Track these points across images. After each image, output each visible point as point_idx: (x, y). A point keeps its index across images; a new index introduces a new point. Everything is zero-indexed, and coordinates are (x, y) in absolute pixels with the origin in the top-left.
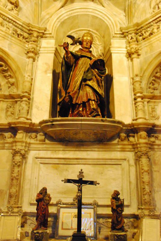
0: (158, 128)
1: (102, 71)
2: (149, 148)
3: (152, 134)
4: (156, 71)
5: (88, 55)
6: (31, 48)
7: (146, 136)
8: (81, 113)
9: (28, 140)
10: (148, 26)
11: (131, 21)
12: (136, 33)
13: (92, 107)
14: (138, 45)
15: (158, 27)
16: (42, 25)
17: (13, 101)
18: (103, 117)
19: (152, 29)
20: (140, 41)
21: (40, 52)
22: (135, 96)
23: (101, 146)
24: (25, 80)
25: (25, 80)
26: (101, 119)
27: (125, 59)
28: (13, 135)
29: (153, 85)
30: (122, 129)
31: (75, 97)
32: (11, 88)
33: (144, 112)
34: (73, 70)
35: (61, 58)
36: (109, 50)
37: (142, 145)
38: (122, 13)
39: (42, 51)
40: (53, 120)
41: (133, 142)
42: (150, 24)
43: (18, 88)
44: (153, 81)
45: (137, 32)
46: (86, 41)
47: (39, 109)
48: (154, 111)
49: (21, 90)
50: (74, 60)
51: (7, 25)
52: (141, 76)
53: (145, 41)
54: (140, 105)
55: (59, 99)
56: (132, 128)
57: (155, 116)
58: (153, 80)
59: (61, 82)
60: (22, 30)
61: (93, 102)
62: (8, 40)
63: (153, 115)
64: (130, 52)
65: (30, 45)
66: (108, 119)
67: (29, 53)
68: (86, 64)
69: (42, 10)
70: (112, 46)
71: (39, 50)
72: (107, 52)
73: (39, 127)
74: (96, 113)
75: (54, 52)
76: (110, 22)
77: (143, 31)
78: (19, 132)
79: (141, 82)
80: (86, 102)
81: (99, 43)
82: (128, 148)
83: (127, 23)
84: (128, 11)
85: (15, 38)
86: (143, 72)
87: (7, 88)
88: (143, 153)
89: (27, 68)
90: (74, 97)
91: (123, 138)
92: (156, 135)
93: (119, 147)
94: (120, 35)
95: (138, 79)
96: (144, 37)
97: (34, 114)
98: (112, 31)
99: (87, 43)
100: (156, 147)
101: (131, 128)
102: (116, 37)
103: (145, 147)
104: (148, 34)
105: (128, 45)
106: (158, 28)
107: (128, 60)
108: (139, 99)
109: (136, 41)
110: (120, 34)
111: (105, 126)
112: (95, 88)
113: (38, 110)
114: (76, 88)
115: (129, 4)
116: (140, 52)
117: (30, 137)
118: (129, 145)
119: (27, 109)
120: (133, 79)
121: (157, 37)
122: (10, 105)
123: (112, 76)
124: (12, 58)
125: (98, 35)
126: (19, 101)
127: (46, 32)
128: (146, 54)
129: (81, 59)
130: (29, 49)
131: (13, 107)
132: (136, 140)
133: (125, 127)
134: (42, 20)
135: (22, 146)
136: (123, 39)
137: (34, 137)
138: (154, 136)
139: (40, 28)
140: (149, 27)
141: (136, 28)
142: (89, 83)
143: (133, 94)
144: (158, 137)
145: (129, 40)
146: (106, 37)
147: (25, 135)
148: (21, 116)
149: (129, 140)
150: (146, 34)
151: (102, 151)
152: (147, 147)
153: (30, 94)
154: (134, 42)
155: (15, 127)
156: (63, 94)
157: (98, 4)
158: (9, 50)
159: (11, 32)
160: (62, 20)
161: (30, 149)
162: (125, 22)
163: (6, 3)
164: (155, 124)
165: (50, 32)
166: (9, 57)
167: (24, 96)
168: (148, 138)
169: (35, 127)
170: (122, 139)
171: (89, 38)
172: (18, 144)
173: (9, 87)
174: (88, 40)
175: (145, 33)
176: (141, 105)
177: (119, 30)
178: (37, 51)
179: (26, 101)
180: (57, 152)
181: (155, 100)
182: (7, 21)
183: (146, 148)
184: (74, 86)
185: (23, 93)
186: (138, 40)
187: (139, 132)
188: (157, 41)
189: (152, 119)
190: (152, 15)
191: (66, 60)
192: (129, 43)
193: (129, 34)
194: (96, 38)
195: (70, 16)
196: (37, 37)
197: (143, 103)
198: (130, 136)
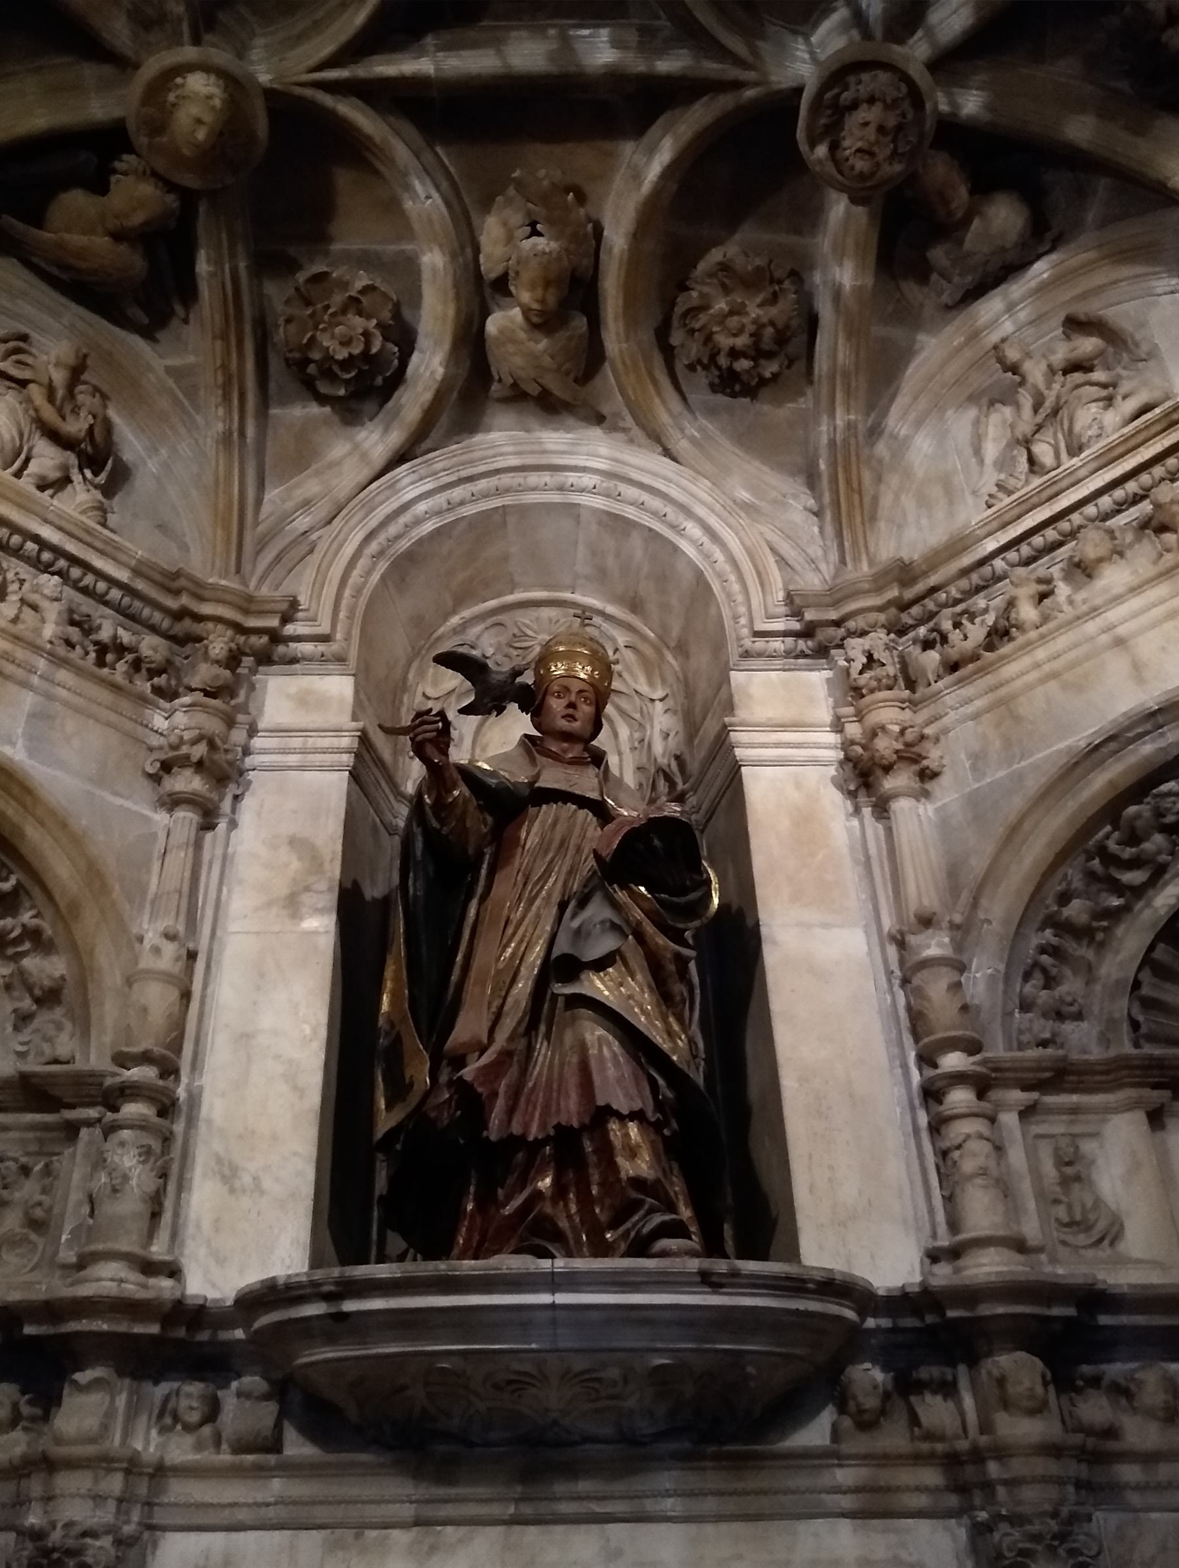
0: (1124, 1320)
1: (684, 892)
2: (1079, 1485)
3: (1086, 1369)
4: (1056, 886)
5: (586, 783)
6: (187, 736)
7: (1039, 1390)
8: (548, 1209)
9: (147, 1442)
10: (975, 578)
11: (855, 543)
12: (899, 627)
13: (627, 1168)
14: (914, 705)
15: (1043, 588)
16: (262, 579)
17: (46, 1127)
18: (713, 1248)
19: (999, 602)
20: (931, 678)
21: (249, 761)
22: (930, 1073)
23: (713, 1479)
24: (142, 965)
25: (142, 965)
26: (694, 1264)
27: (834, 803)
28: (30, 1403)
29: (1050, 982)
30: (854, 1330)
31: (502, 1089)
32: (36, 1023)
33: (1004, 1188)
34: (480, 890)
35: (399, 794)
36: (722, 745)
37: (1018, 1467)
38: (795, 497)
39: (264, 752)
40: (340, 1282)
41: (949, 1432)
42: (986, 570)
43: (84, 1025)
44: (1045, 959)
45: (906, 619)
46: (567, 689)
47: (237, 1184)
48: (1078, 1178)
49: (108, 1039)
50: (490, 819)
51: (26, 586)
52: (953, 927)
53: (960, 680)
54: (968, 1137)
55: (382, 1104)
56: (930, 1319)
57: (1092, 1217)
58: (1042, 950)
59: (397, 979)
60: (133, 618)
61: (633, 1130)
62: (25, 685)
63: (1070, 1207)
64: (866, 755)
65: (180, 718)
66: (751, 1266)
67: (175, 770)
68: (572, 851)
69: (272, 386)
70: (742, 714)
71: (247, 751)
72: (712, 756)
73: (239, 1334)
74: (658, 1219)
75: (347, 759)
76: (718, 555)
77: (948, 612)
78: (83, 1377)
79: (962, 968)
80: (583, 1127)
81: (651, 684)
82: (918, 1489)
83: (834, 556)
84: (834, 480)
85: (79, 671)
86: (965, 897)
87: (10, 1029)
88: (1036, 1538)
89: (154, 880)
90: (494, 1095)
91: (871, 1403)
92: (1115, 1370)
93: (844, 1476)
94: (790, 641)
95: (935, 945)
96: (953, 653)
97: (198, 1227)
98: (736, 618)
99: (572, 705)
100: (1130, 1473)
101: (923, 1319)
102: (760, 655)
103: (1045, 1479)
104: (976, 632)
105: (850, 710)
106: (1043, 597)
107: (857, 811)
108: (960, 1098)
109: (901, 683)
110: (786, 634)
111: (728, 1320)
112: (641, 1022)
113: (232, 1191)
114: (508, 1024)
115: (839, 437)
116: (934, 756)
117: (161, 1415)
118: (917, 1459)
119: (151, 1184)
120: (901, 944)
121: (1041, 654)
122: (24, 1160)
123: (750, 922)
124: (53, 813)
125: (644, 638)
126: (89, 1123)
127: (290, 629)
128: (974, 768)
129: (532, 810)
130: (174, 747)
131: (47, 1171)
132: (972, 1417)
133: (875, 1316)
134: (262, 544)
135: (98, 1499)
136: (810, 669)
137: (194, 1417)
138: (1105, 1383)
139: (250, 599)
140: (984, 587)
141: (893, 593)
142: (599, 986)
143: (912, 1056)
144: (1132, 1387)
145: (854, 674)
146: (701, 660)
147: (129, 1402)
148: (100, 1247)
149: (914, 1420)
150: (966, 638)
151: (719, 1518)
152: (1060, 1482)
153: (169, 1070)
154: (890, 688)
155: (48, 1338)
156: (420, 1072)
157: (631, 441)
158: (31, 752)
159: (49, 630)
160: (404, 544)
161: (159, 1518)
162: (820, 552)
163: (21, 435)
164: (1100, 1286)
165: (324, 628)
166: (28, 800)
167: (128, 1092)
168: (1059, 1392)
169: (204, 1336)
170: (861, 1411)
171: (583, 672)
172: (66, 1482)
173: (22, 1020)
174: (575, 686)
175: (957, 625)
176: (981, 1137)
177: (783, 610)
178: (230, 757)
179: (141, 1126)
180: (372, 1534)
181: (1075, 1098)
182: (27, 560)
183: (1053, 1492)
184: (494, 1009)
185: (123, 1060)
186: (911, 671)
187: (989, 1354)
188: (1043, 681)
189: (1069, 1238)
190: (999, 515)
191: (435, 824)
192: (857, 692)
193: (851, 634)
194: (629, 655)
195: (450, 518)
196: (233, 660)
197: (992, 1120)
198: (920, 1387)
